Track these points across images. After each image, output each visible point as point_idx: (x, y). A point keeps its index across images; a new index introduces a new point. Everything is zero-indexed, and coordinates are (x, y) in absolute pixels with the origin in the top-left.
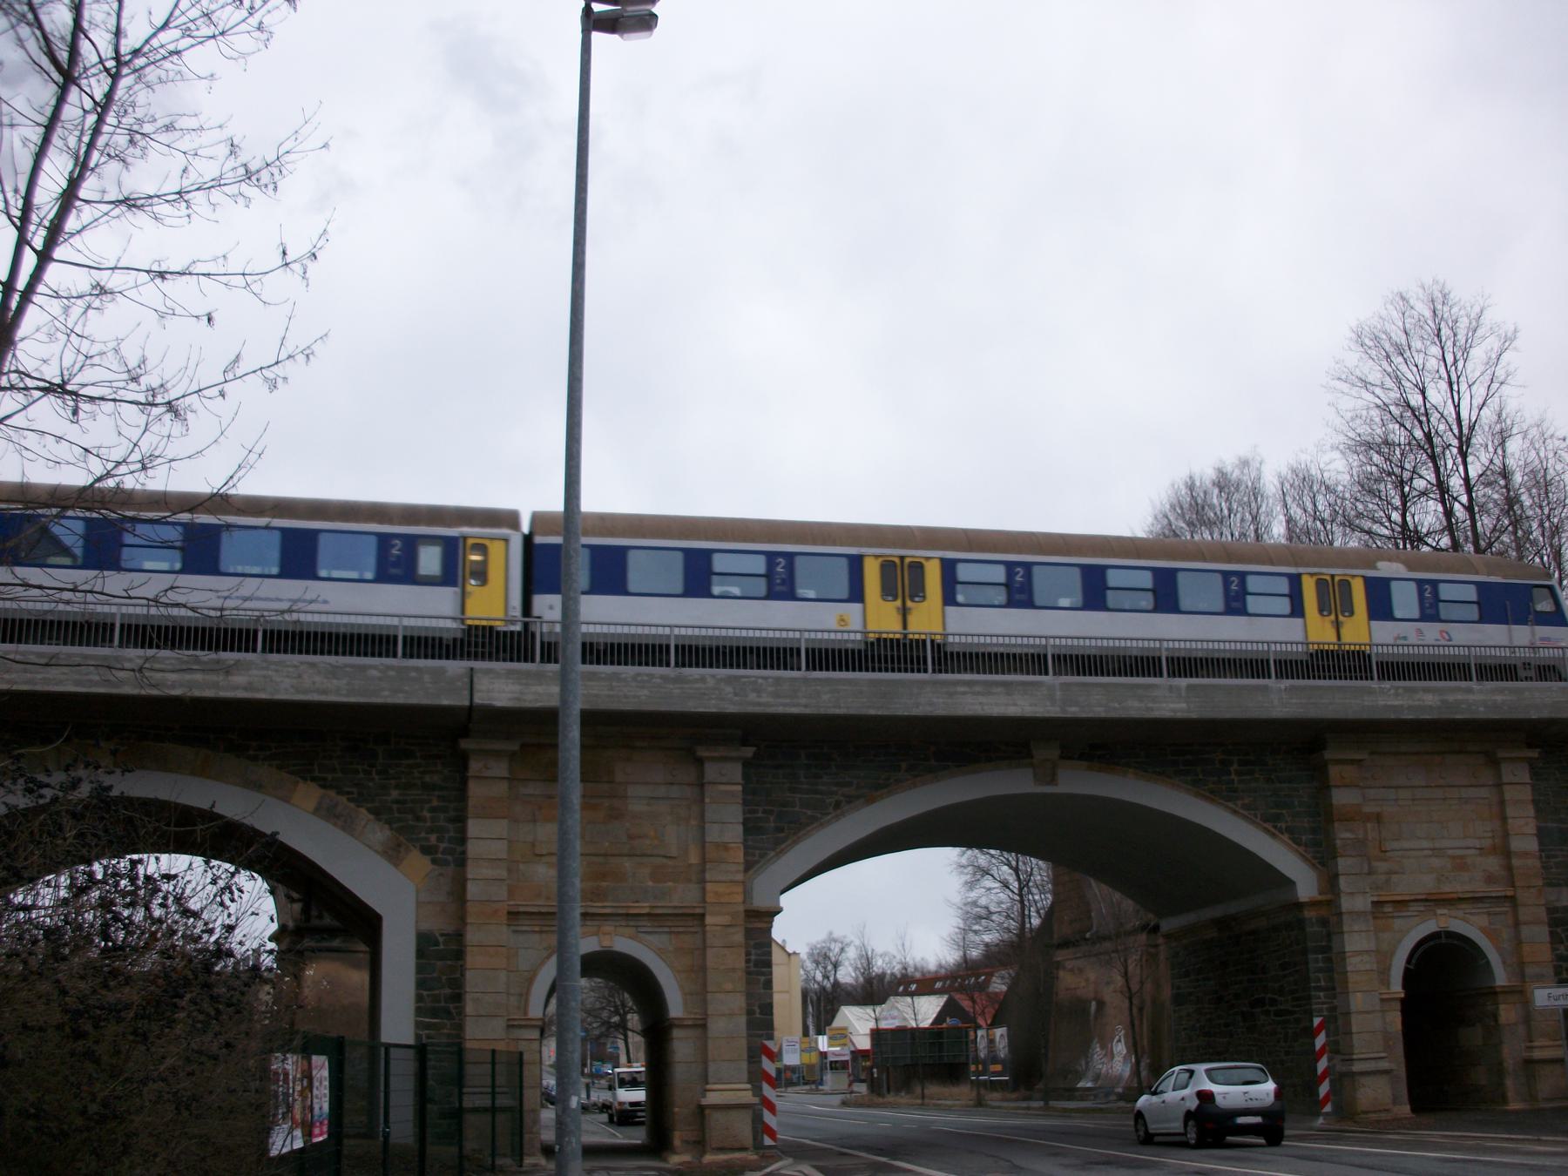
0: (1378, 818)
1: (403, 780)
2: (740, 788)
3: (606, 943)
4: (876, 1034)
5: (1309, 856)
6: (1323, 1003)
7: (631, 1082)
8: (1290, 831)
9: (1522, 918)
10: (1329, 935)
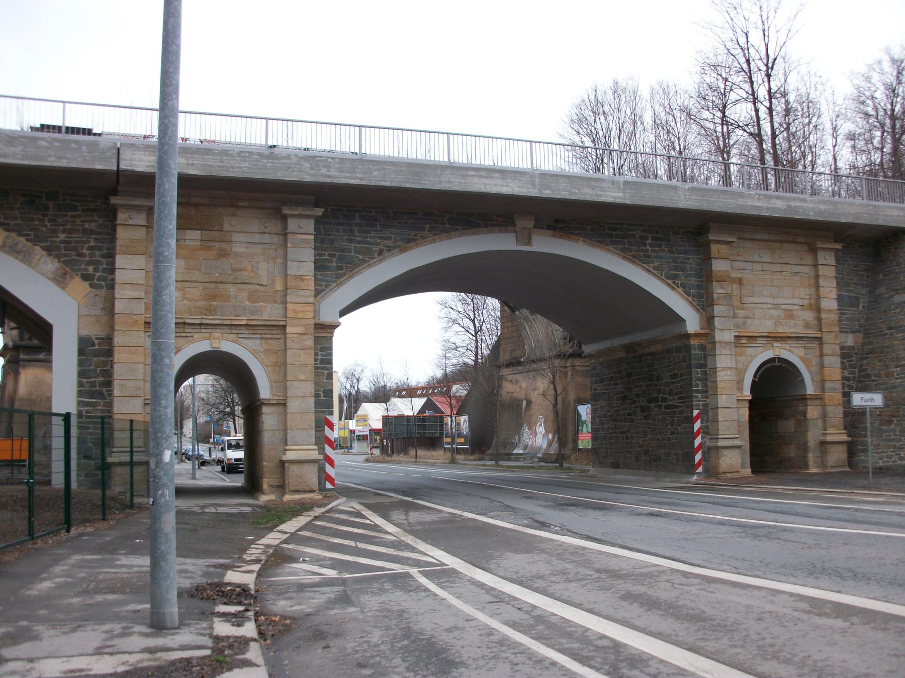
0: (740, 281)
1: (69, 227)
2: (313, 237)
3: (216, 345)
4: (386, 419)
5: (695, 304)
6: (700, 401)
7: (237, 447)
8: (683, 286)
9: (825, 351)
10: (705, 356)
